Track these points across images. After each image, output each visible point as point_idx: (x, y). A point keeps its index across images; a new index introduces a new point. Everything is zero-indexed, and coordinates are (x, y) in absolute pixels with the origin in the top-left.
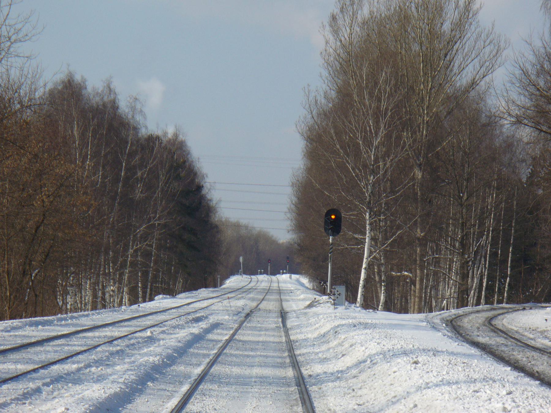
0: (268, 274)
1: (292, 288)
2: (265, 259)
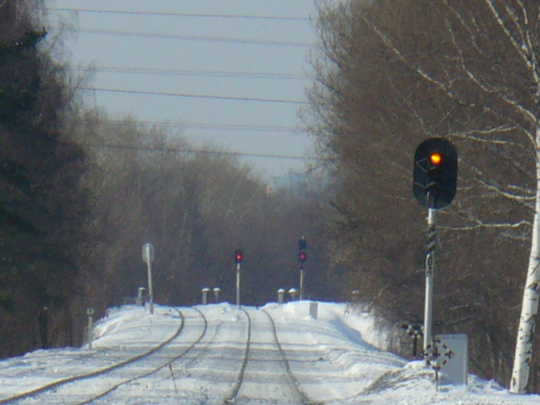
0: (233, 302)
1: (322, 348)
2: (231, 248)
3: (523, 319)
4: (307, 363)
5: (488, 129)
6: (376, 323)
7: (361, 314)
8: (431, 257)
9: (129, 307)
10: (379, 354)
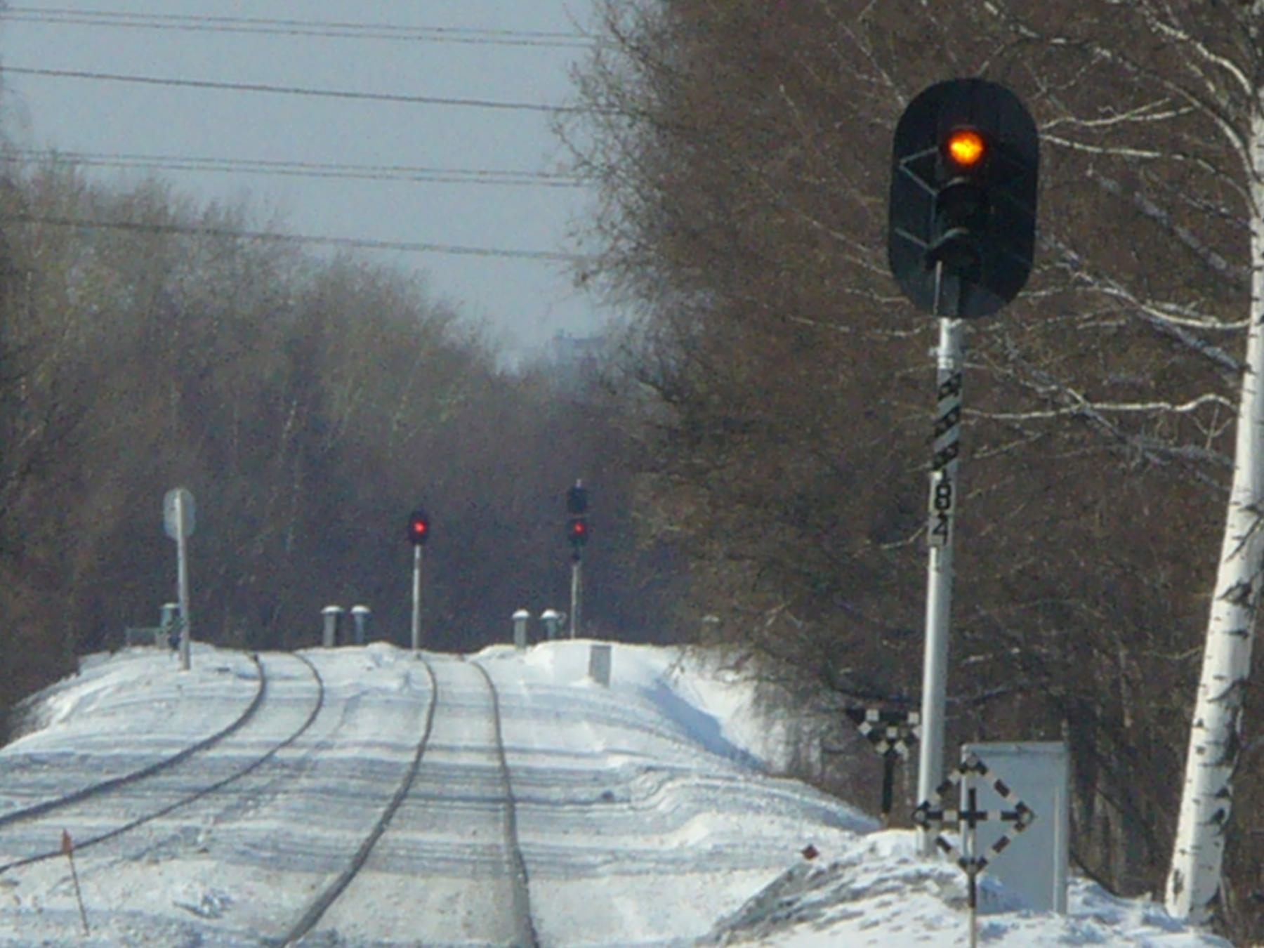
0: (402, 641)
3: (1206, 693)
4: (568, 808)
5: (1108, 115)
6: (757, 701)
7: (723, 672)
8: (944, 483)
9: (139, 650)
10: (764, 785)
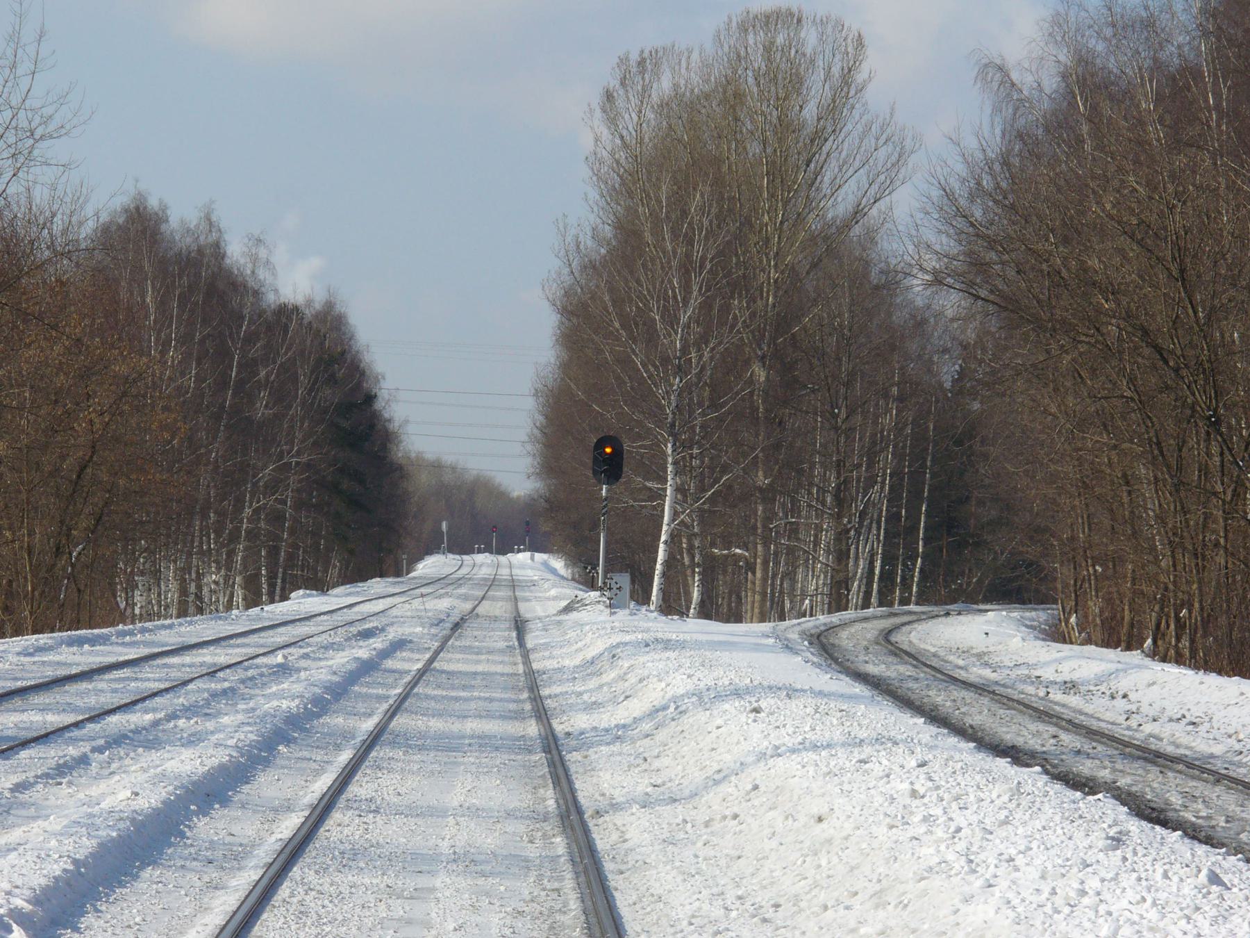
0: (491, 553)
2: (485, 524)
